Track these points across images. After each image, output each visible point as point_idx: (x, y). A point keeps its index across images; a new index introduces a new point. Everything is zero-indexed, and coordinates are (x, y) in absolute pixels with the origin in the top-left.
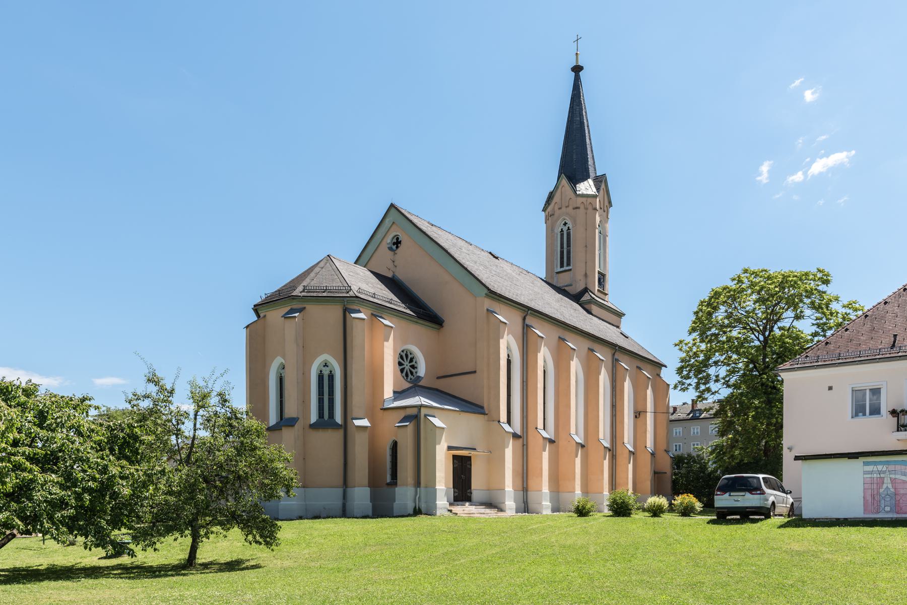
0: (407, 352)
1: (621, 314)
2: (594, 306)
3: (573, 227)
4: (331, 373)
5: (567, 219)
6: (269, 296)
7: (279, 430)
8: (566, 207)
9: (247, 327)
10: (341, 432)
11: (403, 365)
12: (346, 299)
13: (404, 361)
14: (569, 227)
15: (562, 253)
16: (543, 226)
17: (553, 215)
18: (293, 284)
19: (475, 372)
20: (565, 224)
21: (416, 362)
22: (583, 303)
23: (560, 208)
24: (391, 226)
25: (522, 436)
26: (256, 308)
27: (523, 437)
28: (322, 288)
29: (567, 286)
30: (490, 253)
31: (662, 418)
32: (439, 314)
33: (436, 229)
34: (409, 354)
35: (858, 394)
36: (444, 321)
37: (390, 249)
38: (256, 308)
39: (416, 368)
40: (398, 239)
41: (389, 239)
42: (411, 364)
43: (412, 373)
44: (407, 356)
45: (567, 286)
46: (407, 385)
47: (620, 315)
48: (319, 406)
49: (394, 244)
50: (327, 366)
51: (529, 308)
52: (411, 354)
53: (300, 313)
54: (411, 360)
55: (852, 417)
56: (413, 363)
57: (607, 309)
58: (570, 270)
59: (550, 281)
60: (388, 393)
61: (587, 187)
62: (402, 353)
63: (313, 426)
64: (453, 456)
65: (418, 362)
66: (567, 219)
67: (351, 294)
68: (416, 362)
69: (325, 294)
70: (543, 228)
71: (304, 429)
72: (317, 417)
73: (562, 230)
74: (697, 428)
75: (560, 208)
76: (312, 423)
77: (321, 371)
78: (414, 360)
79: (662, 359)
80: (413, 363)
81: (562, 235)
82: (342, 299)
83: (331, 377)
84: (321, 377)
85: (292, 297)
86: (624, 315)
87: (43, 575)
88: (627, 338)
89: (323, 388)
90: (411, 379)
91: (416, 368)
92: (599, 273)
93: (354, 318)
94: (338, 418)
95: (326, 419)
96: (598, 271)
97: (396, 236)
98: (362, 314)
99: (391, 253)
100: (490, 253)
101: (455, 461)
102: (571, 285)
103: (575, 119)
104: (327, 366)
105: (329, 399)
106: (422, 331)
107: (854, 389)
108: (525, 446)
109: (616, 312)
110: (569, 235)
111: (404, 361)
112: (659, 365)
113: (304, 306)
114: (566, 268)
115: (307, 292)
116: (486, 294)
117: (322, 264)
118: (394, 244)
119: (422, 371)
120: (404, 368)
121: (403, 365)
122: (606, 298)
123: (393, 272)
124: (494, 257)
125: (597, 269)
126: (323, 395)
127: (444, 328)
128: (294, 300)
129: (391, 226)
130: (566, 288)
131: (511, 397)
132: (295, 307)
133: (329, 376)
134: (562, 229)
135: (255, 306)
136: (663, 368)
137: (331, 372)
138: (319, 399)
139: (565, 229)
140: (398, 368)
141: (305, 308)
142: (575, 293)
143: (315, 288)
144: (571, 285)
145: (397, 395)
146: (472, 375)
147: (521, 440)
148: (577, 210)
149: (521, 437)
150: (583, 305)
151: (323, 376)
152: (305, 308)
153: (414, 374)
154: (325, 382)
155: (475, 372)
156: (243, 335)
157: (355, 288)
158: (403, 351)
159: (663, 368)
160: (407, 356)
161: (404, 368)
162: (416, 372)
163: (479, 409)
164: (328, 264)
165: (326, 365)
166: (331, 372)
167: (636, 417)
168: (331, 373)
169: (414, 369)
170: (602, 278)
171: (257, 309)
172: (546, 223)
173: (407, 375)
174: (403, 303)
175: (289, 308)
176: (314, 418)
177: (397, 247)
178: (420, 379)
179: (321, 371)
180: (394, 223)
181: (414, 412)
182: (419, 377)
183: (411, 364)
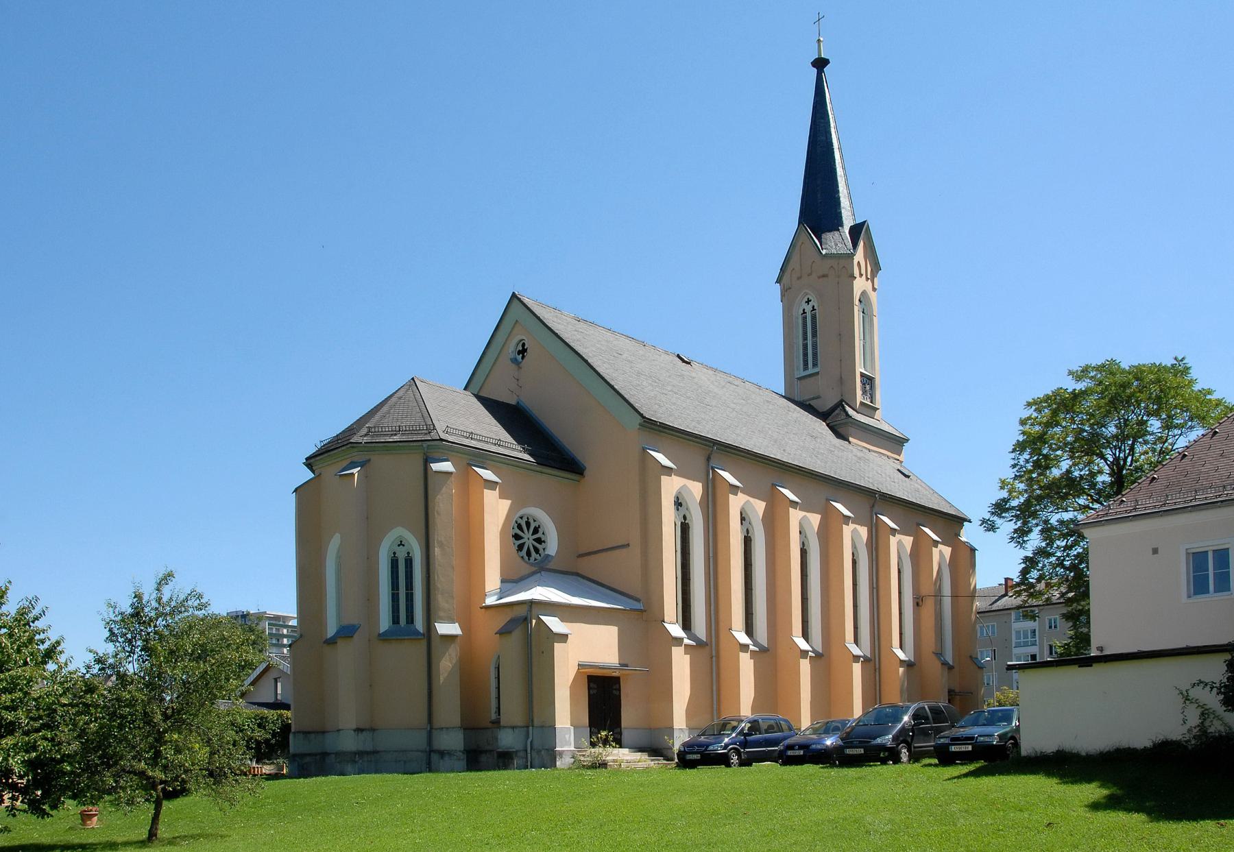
0: (528, 518)
1: (901, 440)
2: (853, 429)
3: (819, 306)
4: (408, 556)
5: (809, 292)
6: (326, 444)
7: (349, 637)
8: (808, 275)
9: (296, 490)
10: (424, 643)
11: (521, 538)
12: (425, 445)
13: (523, 532)
14: (813, 307)
15: (805, 347)
16: (779, 306)
17: (790, 288)
18: (351, 431)
19: (628, 545)
20: (808, 301)
21: (543, 534)
22: (836, 425)
23: (799, 278)
24: (514, 327)
25: (709, 642)
26: (309, 462)
27: (711, 645)
28: (387, 430)
29: (813, 399)
30: (678, 356)
31: (623, 567)
32: (580, 456)
33: (585, 326)
34: (531, 521)
35: (1198, 560)
36: (586, 468)
37: (514, 361)
38: (309, 462)
39: (544, 542)
40: (523, 345)
41: (512, 348)
42: (536, 536)
43: (537, 550)
44: (528, 524)
45: (813, 399)
46: (526, 569)
47: (901, 442)
48: (393, 606)
49: (519, 352)
50: (404, 545)
51: (715, 443)
52: (535, 521)
53: (362, 467)
54: (536, 531)
55: (1189, 597)
56: (539, 535)
57: (875, 432)
58: (817, 373)
59: (790, 397)
60: (492, 579)
61: (836, 242)
62: (519, 521)
63: (384, 637)
64: (1036, 655)
65: (546, 532)
66: (809, 292)
67: (434, 435)
68: (543, 534)
69: (396, 438)
70: (778, 307)
71: (369, 640)
72: (389, 622)
73: (804, 312)
74: (993, 626)
75: (799, 278)
76: (382, 631)
77: (394, 553)
78: (541, 530)
79: (965, 511)
80: (539, 535)
81: (805, 319)
82: (420, 443)
83: (409, 562)
84: (394, 563)
85: (350, 445)
86: (907, 440)
87: (129, 844)
88: (908, 477)
89: (397, 578)
90: (535, 560)
91: (544, 542)
92: (862, 375)
93: (435, 472)
94: (419, 624)
95: (402, 626)
96: (862, 375)
97: (521, 341)
98: (450, 463)
99: (514, 366)
100: (678, 356)
101: (592, 685)
102: (818, 397)
103: (819, 138)
104: (404, 545)
105: (407, 594)
106: (553, 482)
107: (1189, 551)
108: (714, 659)
109: (892, 436)
110: (814, 318)
111: (523, 532)
112: (957, 521)
113: (367, 458)
114: (811, 371)
115: (372, 436)
116: (640, 425)
117: (400, 394)
118: (519, 352)
119: (552, 546)
120: (534, 540)
121: (521, 538)
122: (878, 414)
123: (518, 396)
124: (683, 361)
125: (860, 369)
126: (398, 589)
127: (586, 478)
128: (356, 450)
129: (514, 327)
130: (812, 403)
131: (808, 578)
132: (355, 459)
133: (406, 560)
134: (804, 310)
135: (307, 459)
136: (965, 523)
137: (408, 553)
138: (393, 594)
139: (808, 308)
140: (512, 545)
141: (369, 460)
142: (825, 410)
143: (384, 430)
144: (818, 397)
145: (509, 585)
146: (624, 550)
147: (708, 648)
148: (824, 279)
149: (707, 645)
150: (836, 427)
151: (397, 560)
152: (369, 460)
153: (541, 551)
154: (401, 569)
155: (628, 545)
156: (291, 501)
157: (440, 427)
158: (521, 518)
159: (965, 523)
160: (528, 524)
161: (534, 540)
162: (544, 549)
163: (635, 602)
164: (410, 392)
165: (401, 544)
166: (408, 553)
167: (918, 604)
168: (408, 556)
169: (541, 544)
170: (868, 381)
171: (310, 463)
172: (782, 301)
173: (529, 554)
174: (519, 442)
175: (348, 461)
176: (385, 623)
177: (523, 358)
178: (550, 558)
179: (394, 553)
180: (517, 321)
181: (521, 612)
182: (548, 556)
183: (536, 536)
